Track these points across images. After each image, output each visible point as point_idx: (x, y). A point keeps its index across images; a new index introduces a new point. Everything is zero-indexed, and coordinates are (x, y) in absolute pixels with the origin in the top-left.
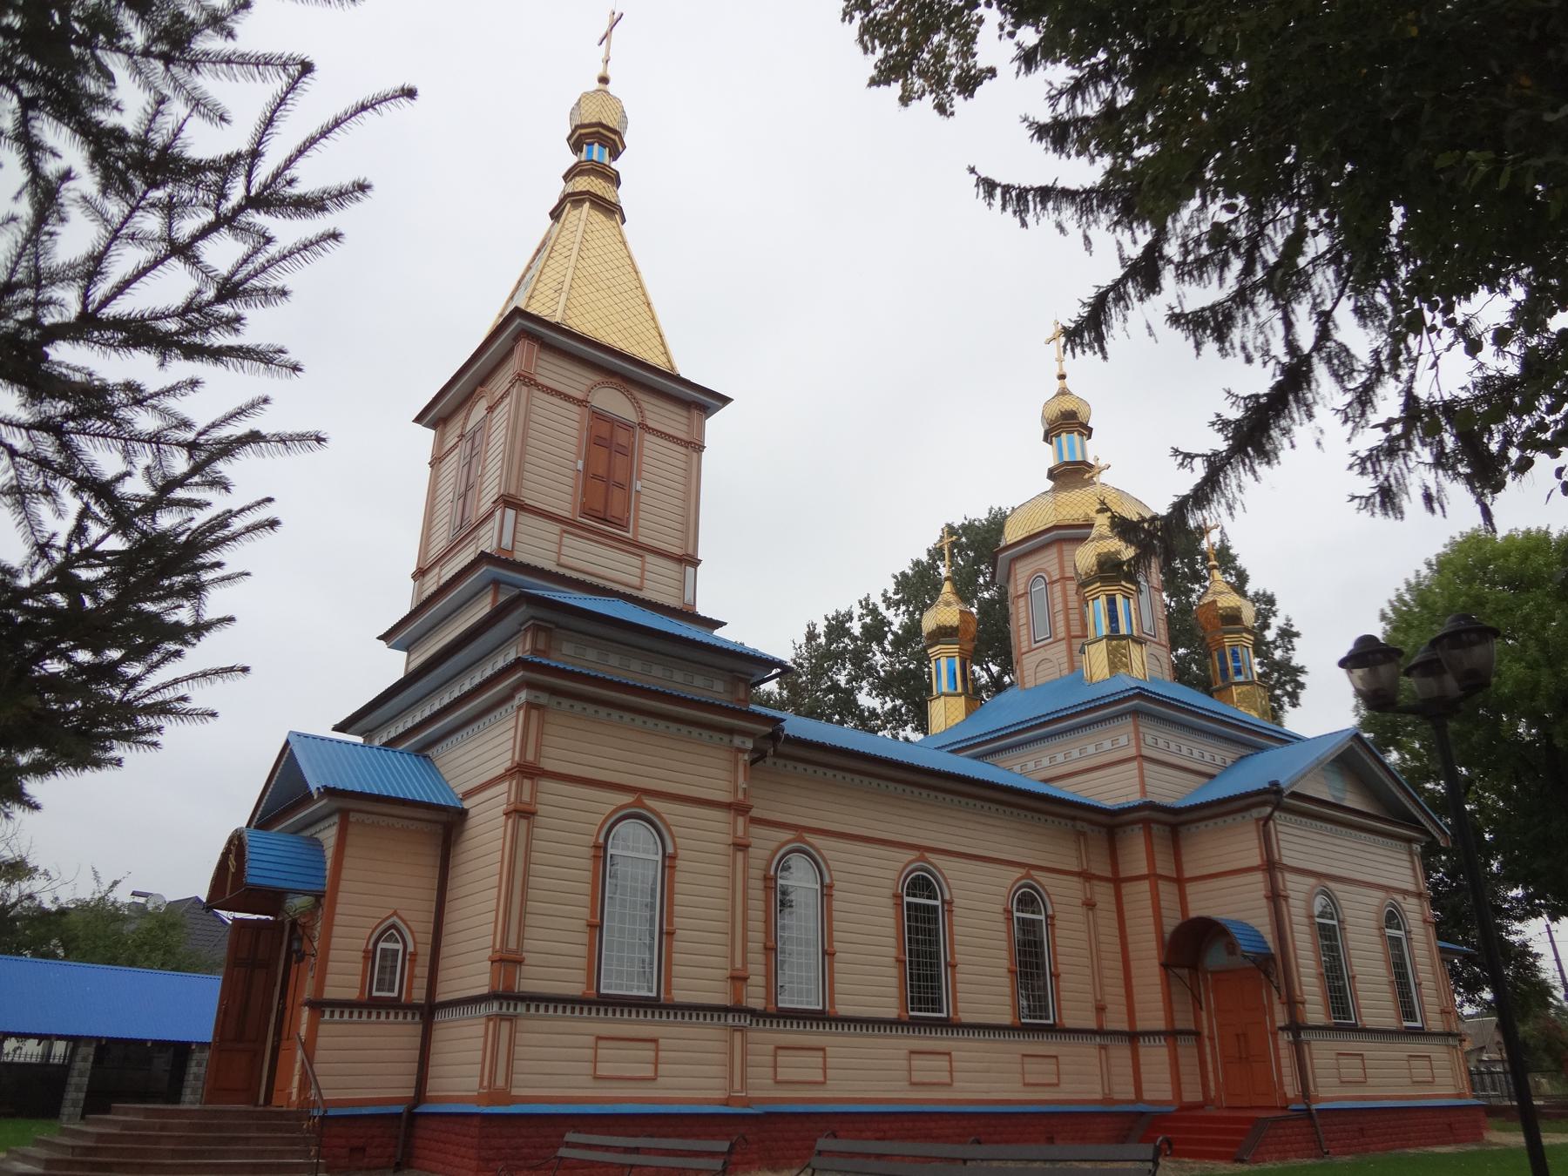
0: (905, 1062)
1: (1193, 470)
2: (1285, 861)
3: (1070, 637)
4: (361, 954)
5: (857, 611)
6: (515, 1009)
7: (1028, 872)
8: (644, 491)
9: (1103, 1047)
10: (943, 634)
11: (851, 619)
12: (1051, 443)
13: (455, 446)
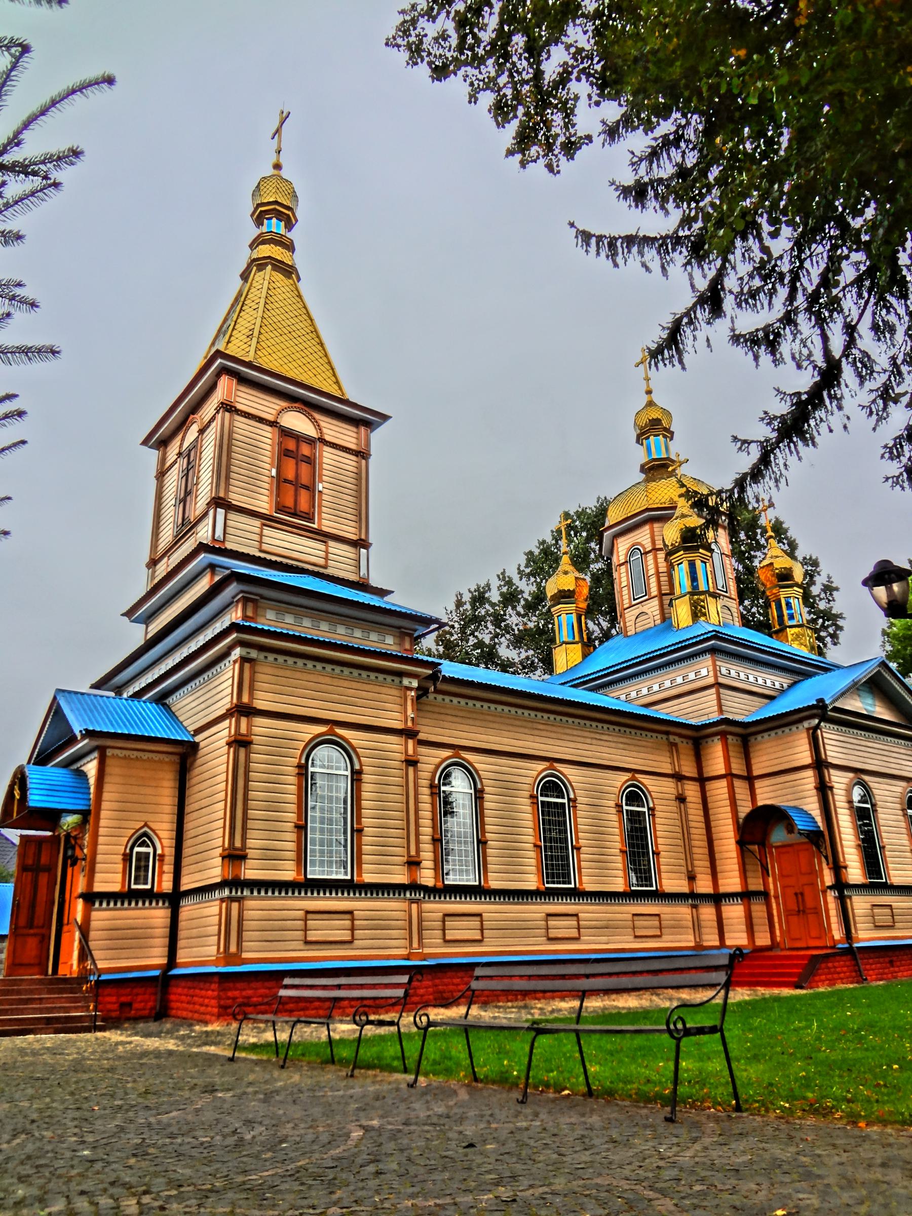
0: (543, 923)
1: (749, 453)
2: (830, 760)
3: (661, 595)
4: (121, 857)
5: (495, 583)
6: (242, 893)
7: (633, 776)
8: (325, 491)
9: (694, 906)
10: (564, 596)
11: (490, 590)
12: (642, 444)
13: (175, 462)
